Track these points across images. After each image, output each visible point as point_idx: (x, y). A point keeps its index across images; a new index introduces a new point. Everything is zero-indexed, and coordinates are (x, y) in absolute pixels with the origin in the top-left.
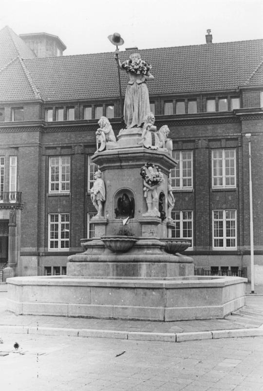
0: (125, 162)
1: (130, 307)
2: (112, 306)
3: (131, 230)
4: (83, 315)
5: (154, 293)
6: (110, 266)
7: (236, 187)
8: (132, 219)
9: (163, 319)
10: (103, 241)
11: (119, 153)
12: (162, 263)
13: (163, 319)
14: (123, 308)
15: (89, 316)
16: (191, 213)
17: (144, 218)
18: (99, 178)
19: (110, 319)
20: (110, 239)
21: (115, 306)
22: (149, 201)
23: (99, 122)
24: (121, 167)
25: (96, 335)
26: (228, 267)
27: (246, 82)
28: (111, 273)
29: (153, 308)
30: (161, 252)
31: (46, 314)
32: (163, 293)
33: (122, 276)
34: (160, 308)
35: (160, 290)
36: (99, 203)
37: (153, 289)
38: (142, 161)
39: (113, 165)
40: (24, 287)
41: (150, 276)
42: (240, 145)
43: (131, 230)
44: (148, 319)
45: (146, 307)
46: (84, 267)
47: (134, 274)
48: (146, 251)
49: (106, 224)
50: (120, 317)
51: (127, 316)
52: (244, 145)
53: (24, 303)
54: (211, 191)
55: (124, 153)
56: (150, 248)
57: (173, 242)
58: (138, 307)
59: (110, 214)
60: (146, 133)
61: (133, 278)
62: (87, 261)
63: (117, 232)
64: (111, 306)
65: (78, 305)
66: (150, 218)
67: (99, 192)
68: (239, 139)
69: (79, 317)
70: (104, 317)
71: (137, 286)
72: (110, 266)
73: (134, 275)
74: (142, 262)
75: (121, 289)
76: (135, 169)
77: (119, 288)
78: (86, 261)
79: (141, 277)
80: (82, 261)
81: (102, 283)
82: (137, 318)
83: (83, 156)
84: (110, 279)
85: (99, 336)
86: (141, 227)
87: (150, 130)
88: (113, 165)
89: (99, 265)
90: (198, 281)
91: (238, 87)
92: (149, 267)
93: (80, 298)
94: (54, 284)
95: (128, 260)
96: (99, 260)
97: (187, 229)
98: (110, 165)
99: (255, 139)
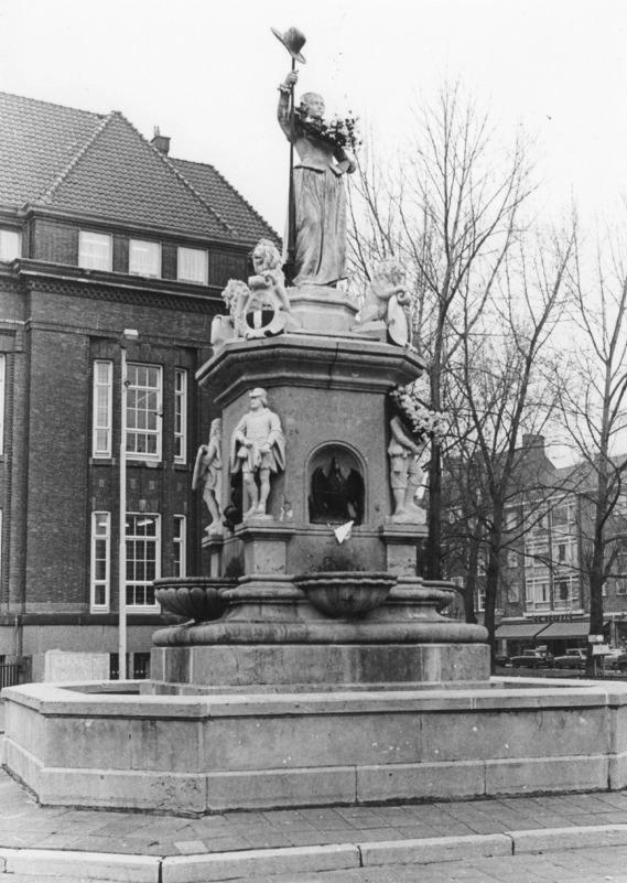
0: (342, 374)
1: (527, 760)
2: (481, 763)
3: (355, 556)
4: (402, 795)
5: (582, 720)
6: (345, 655)
7: (109, 457)
8: (357, 528)
9: (606, 786)
10: (299, 587)
11: (341, 347)
12: (478, 645)
13: (606, 786)
14: (511, 766)
15: (418, 796)
16: (178, 521)
17: (398, 528)
18: (265, 406)
19: (477, 798)
20: (361, 581)
21: (489, 762)
24: (328, 386)
25: (561, 844)
27: (45, 198)
28: (347, 677)
29: (580, 758)
30: (438, 617)
31: (288, 803)
32: (603, 717)
33: (378, 681)
34: (597, 757)
35: (597, 712)
36: (265, 476)
37: (517, 711)
38: (387, 379)
39: (309, 376)
40: (211, 723)
41: (451, 679)
43: (355, 556)
44: (573, 788)
45: (567, 759)
46: (268, 659)
47: (409, 672)
48: (409, 614)
49: (286, 538)
50: (503, 791)
51: (522, 786)
53: (210, 775)
54: (91, 462)
55: (354, 349)
56: (420, 606)
57: (208, 590)
58: (547, 760)
59: (295, 513)
61: (409, 684)
62: (273, 642)
63: (320, 562)
64: (478, 762)
65: (388, 767)
66: (415, 529)
68: (17, 334)
69: (389, 803)
70: (461, 795)
71: (544, 705)
72: (345, 655)
73: (409, 677)
74: (428, 641)
75: (504, 715)
76: (363, 395)
77: (499, 711)
78: (270, 641)
79: (424, 683)
80: (257, 642)
81: (452, 700)
82: (545, 789)
85: (568, 845)
86: (385, 550)
88: (309, 376)
89: (312, 654)
90: (243, 698)
91: (27, 206)
92: (446, 657)
93: (391, 748)
94: (312, 711)
95: (392, 636)
96: (312, 637)
97: (135, 560)
98: (301, 375)
99: (63, 341)
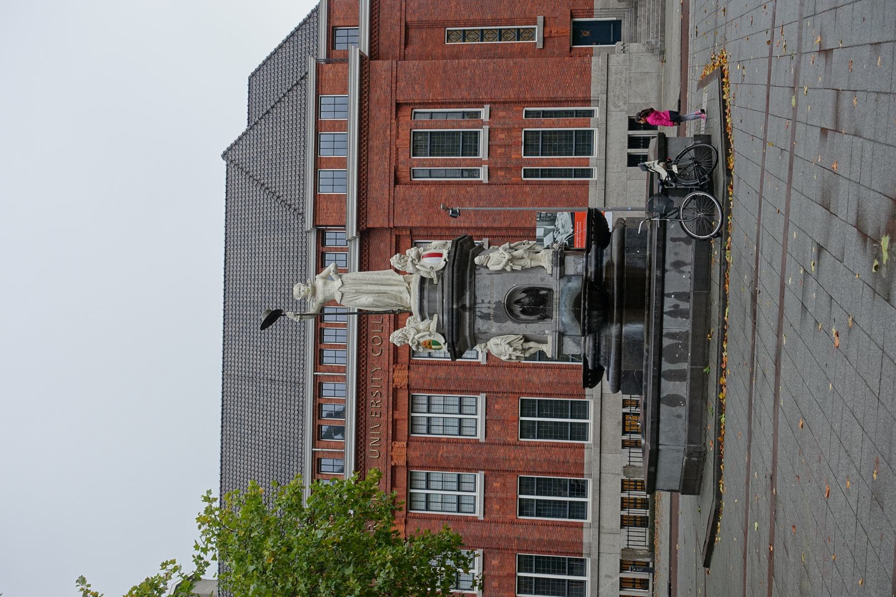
22: (528, 263)
23: (398, 345)
26: (622, 498)
36: (527, 345)
42: (408, 232)
52: (410, 225)
60: (423, 266)
67: (509, 343)
83: (410, 521)
84: (647, 369)
87: (419, 260)
